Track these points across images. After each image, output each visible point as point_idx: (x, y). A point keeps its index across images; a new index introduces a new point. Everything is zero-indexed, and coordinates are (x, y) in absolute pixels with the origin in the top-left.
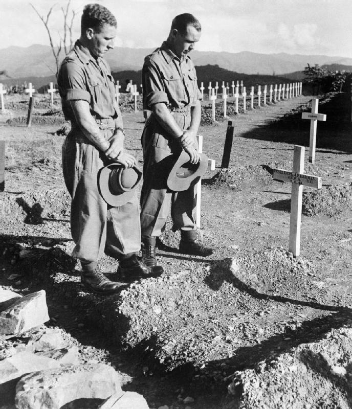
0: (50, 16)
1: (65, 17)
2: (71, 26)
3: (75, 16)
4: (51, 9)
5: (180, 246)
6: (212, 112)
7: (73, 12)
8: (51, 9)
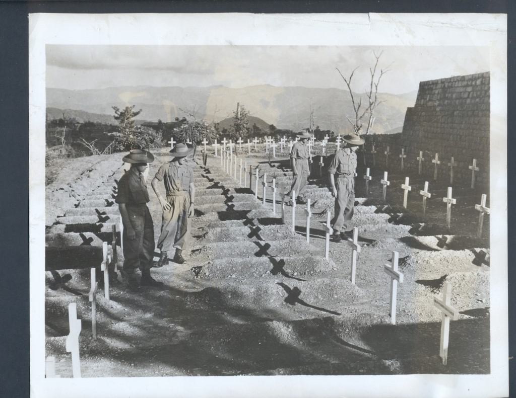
0: (352, 78)
1: (373, 76)
2: (378, 84)
3: (383, 75)
4: (353, 72)
5: (120, 181)
6: (310, 225)
7: (382, 72)
8: (353, 72)
